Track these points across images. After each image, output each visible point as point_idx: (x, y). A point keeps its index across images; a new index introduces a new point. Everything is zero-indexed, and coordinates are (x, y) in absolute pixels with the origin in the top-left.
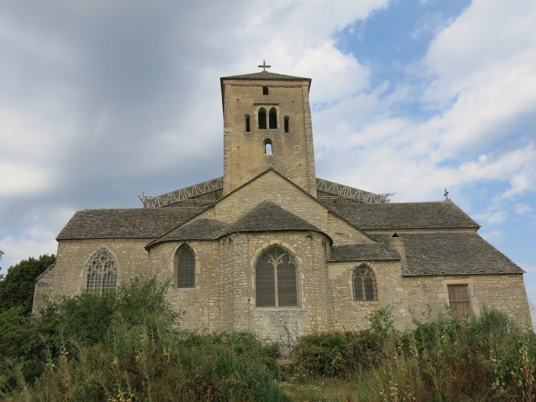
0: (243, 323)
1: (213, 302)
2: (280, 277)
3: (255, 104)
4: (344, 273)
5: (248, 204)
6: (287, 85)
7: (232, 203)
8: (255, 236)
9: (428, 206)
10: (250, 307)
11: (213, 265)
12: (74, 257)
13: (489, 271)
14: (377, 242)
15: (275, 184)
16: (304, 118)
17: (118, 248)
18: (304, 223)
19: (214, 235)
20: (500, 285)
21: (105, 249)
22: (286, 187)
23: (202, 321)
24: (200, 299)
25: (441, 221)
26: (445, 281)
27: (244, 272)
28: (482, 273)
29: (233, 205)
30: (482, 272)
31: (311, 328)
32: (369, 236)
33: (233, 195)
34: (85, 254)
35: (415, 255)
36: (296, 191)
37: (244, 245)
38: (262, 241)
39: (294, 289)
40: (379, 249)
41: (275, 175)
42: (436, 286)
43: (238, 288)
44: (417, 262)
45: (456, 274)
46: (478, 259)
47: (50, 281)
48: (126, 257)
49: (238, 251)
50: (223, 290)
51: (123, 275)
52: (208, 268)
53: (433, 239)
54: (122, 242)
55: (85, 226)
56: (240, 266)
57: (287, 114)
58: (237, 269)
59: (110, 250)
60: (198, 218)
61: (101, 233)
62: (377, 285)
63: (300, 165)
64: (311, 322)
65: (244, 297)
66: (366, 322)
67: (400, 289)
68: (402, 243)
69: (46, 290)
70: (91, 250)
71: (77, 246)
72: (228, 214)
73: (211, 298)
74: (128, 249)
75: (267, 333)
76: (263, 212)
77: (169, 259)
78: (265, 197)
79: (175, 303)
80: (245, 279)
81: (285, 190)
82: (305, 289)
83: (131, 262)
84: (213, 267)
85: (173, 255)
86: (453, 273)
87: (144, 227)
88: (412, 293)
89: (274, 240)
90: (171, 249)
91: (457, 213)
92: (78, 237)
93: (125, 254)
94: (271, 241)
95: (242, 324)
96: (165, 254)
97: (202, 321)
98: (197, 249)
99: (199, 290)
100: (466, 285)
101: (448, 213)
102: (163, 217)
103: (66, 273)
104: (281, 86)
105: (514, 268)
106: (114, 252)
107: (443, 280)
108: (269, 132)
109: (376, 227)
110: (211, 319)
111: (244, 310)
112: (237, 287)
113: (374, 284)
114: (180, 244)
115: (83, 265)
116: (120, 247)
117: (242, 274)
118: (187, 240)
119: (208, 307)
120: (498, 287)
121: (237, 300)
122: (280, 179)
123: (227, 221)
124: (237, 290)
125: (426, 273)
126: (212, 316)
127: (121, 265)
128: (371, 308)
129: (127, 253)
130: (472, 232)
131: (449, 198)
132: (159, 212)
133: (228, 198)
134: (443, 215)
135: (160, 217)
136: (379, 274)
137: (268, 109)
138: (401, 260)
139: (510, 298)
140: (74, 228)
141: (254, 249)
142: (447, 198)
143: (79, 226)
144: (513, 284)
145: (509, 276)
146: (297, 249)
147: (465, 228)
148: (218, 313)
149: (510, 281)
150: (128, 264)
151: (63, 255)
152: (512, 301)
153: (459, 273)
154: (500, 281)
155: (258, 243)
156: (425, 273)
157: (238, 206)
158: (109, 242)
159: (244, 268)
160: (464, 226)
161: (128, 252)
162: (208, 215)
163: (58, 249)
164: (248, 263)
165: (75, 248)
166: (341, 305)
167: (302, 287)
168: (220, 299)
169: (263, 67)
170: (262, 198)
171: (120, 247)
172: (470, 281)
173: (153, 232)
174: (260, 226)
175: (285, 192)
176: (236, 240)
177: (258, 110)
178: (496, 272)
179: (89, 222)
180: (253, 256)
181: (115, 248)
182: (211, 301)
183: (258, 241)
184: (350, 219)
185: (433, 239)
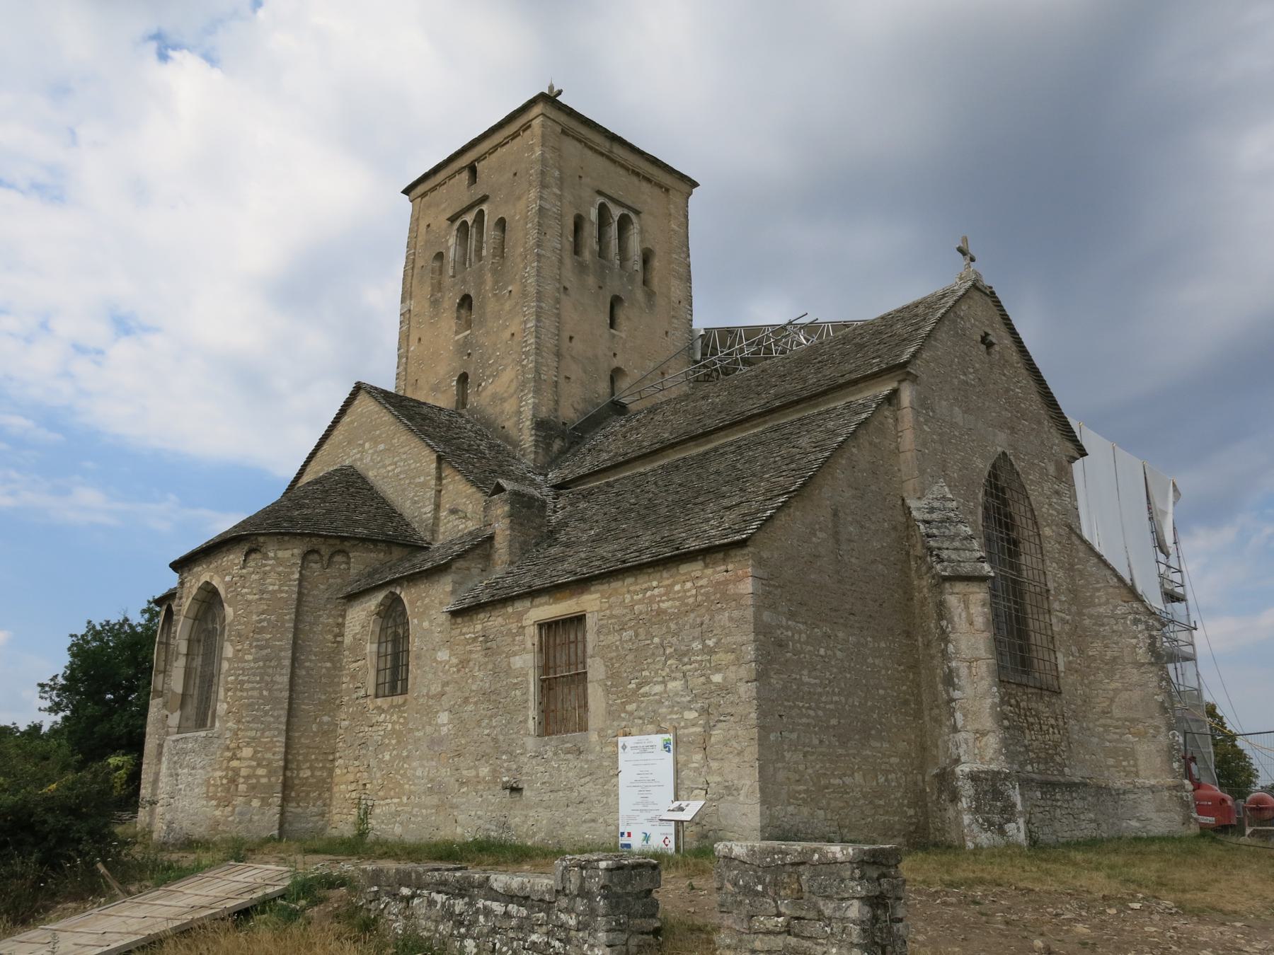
6: (505, 139)
20: (670, 603)
31: (225, 777)
42: (509, 632)
64: (229, 762)
82: (227, 682)
88: (464, 663)
120: (664, 612)
130: (538, 433)
139: (697, 645)
144: (711, 590)
145: (704, 560)
146: (228, 586)
149: (703, 582)
152: (699, 658)
154: (673, 585)
163: (1076, 500)
167: (222, 677)
172: (590, 603)
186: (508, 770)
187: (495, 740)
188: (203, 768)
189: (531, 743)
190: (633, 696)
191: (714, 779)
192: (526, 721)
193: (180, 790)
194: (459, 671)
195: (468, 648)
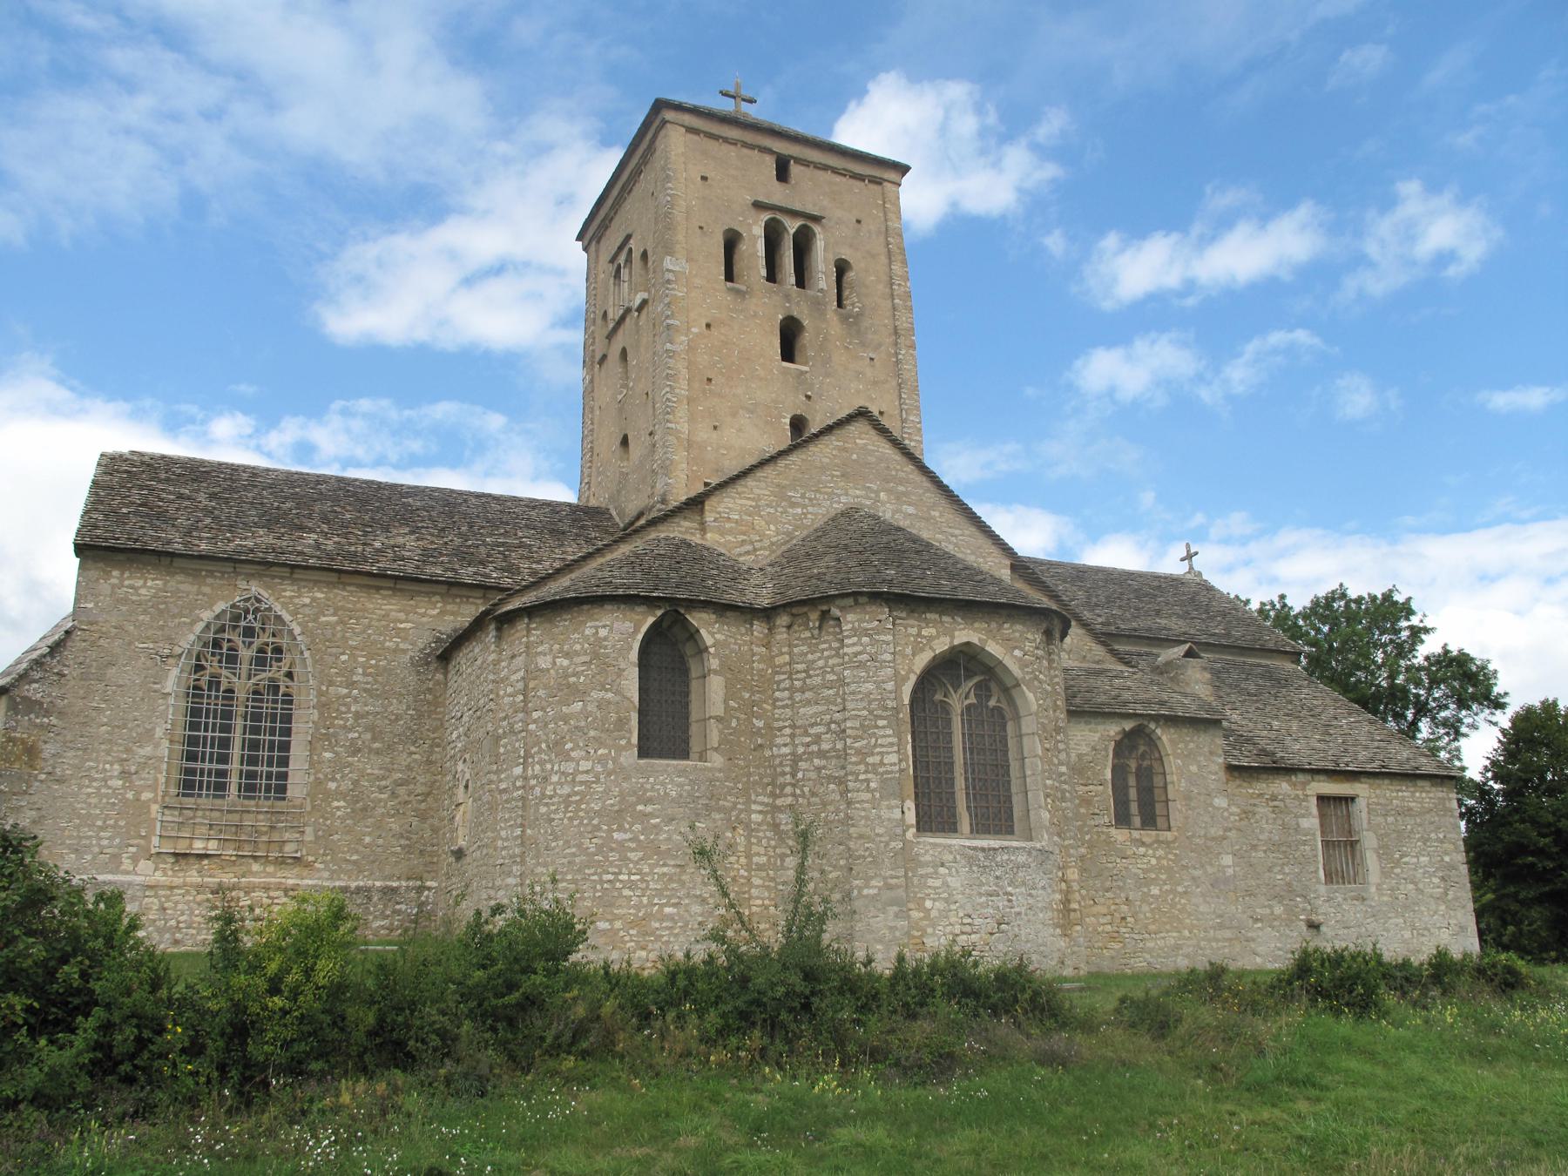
0: (890, 881)
1: (760, 812)
4: (1094, 749)
5: (799, 510)
7: (753, 499)
8: (913, 611)
10: (904, 831)
11: (759, 692)
12: (141, 618)
15: (874, 460)
16: (891, 278)
17: (307, 601)
21: (259, 601)
22: (902, 474)
23: (733, 869)
24: (725, 799)
26: (1314, 784)
27: (885, 722)
29: (757, 506)
32: (1113, 653)
33: (760, 474)
34: (186, 612)
36: (928, 490)
37: (883, 638)
38: (933, 631)
41: (873, 432)
43: (866, 772)
47: (50, 695)
48: (334, 635)
49: (860, 653)
50: (793, 775)
51: (323, 699)
52: (744, 700)
54: (320, 582)
56: (870, 703)
57: (846, 254)
58: (859, 710)
59: (277, 608)
62: (1170, 787)
65: (888, 799)
66: (1145, 890)
67: (1221, 802)
69: (36, 725)
70: (206, 598)
71: (153, 580)
72: (744, 533)
73: (753, 797)
74: (342, 608)
75: (961, 914)
77: (621, 659)
78: (847, 494)
79: (649, 809)
80: (891, 745)
81: (901, 482)
82: (1045, 785)
83: (353, 657)
84: (757, 697)
85: (636, 646)
88: (1247, 814)
89: (966, 633)
90: (628, 624)
93: (333, 626)
94: (957, 633)
95: (886, 884)
96: (605, 639)
97: (733, 869)
98: (713, 634)
99: (720, 770)
100: (1353, 799)
103: (111, 671)
106: (294, 613)
107: (1308, 783)
110: (757, 864)
111: (891, 840)
112: (862, 768)
113: (1158, 781)
114: (659, 613)
115: (178, 650)
116: (314, 599)
117: (877, 727)
119: (747, 826)
121: (864, 810)
122: (886, 449)
123: (740, 555)
124: (862, 777)
126: (758, 854)
127: (315, 662)
128: (1157, 849)
129: (337, 623)
131: (1196, 568)
133: (742, 482)
136: (1177, 756)
137: (792, 226)
141: (909, 651)
142: (1191, 568)
143: (140, 505)
148: (775, 848)
149: (1431, 795)
150: (343, 663)
151: (96, 604)
155: (919, 635)
157: (772, 511)
158: (273, 577)
159: (886, 709)
161: (341, 622)
163: (78, 582)
164: (897, 691)
165: (144, 585)
166: (1087, 837)
168: (779, 802)
169: (734, 97)
170: (839, 496)
171: (314, 599)
172: (1360, 789)
175: (901, 488)
176: (850, 617)
180: (908, 673)
181: (296, 601)
182: (754, 807)
183: (920, 628)
186: (1304, 910)
187: (1289, 884)
188: (1044, 888)
189: (1322, 889)
190: (1397, 863)
191: (1453, 922)
192: (1316, 872)
193: (1019, 914)
194: (1241, 819)
195: (1252, 801)
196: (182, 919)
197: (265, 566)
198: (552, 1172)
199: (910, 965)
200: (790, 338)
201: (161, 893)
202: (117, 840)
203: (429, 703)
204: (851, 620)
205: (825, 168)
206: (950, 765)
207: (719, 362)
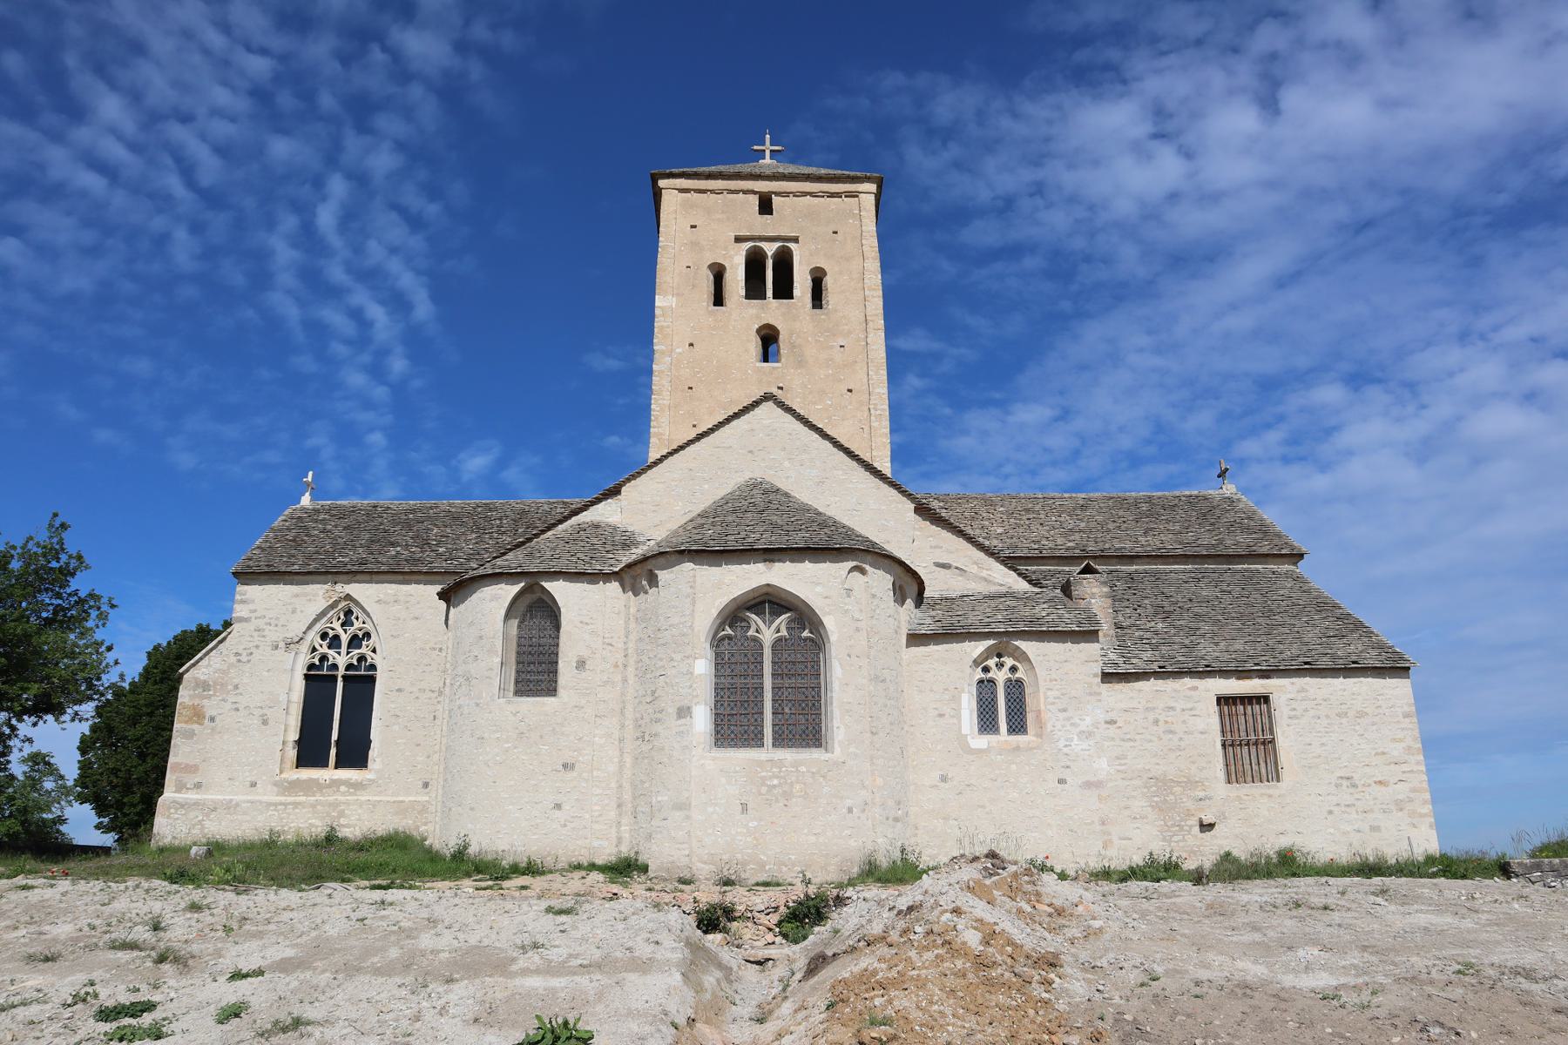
2: (551, 675)
3: (738, 240)
9: (1176, 502)
13: (1325, 662)
14: (1041, 587)
18: (849, 533)
19: (612, 562)
25: (1206, 540)
28: (1306, 666)
30: (1306, 663)
35: (1138, 622)
39: (814, 705)
40: (1045, 606)
44: (1142, 639)
45: (1240, 669)
46: (1298, 632)
53: (1186, 582)
55: (306, 543)
60: (574, 520)
61: (341, 559)
63: (850, 391)
68: (1106, 589)
76: (740, 505)
86: (1232, 667)
87: (450, 546)
91: (1249, 518)
92: (283, 569)
101: (1225, 520)
102: (498, 522)
104: (805, 194)
105: (1389, 655)
108: (771, 310)
109: (1041, 552)
118: (539, 572)
125: (1163, 667)
132: (490, 510)
134: (1212, 524)
135: (493, 522)
137: (770, 249)
138: (1100, 633)
140: (278, 545)
147: (1267, 555)
153: (1249, 666)
156: (1160, 667)
160: (1265, 550)
162: (605, 513)
172: (1282, 690)
173: (468, 560)
174: (729, 538)
177: (744, 253)
178: (1340, 663)
179: (316, 532)
184: (978, 532)
185: (1186, 582)
196: (292, 825)
197: (353, 575)
198: (1362, 1044)
199: (472, 850)
200: (769, 339)
201: (279, 807)
202: (255, 772)
203: (1186, 647)
204: (663, 575)
205: (805, 194)
206: (760, 688)
207: (698, 372)
